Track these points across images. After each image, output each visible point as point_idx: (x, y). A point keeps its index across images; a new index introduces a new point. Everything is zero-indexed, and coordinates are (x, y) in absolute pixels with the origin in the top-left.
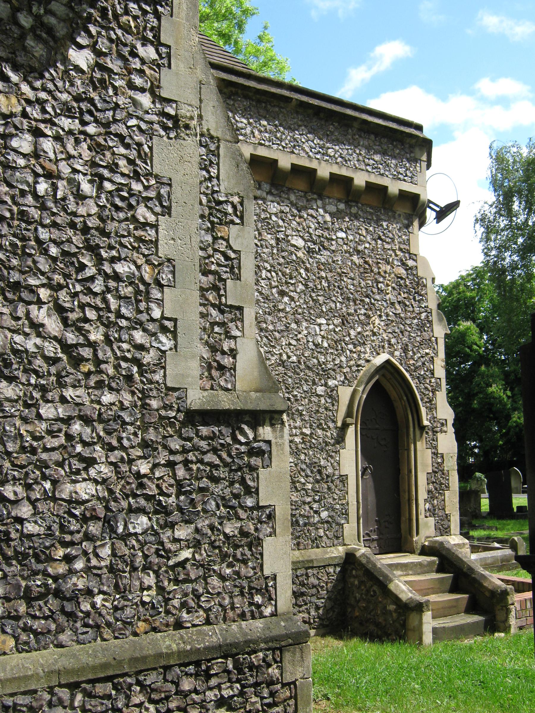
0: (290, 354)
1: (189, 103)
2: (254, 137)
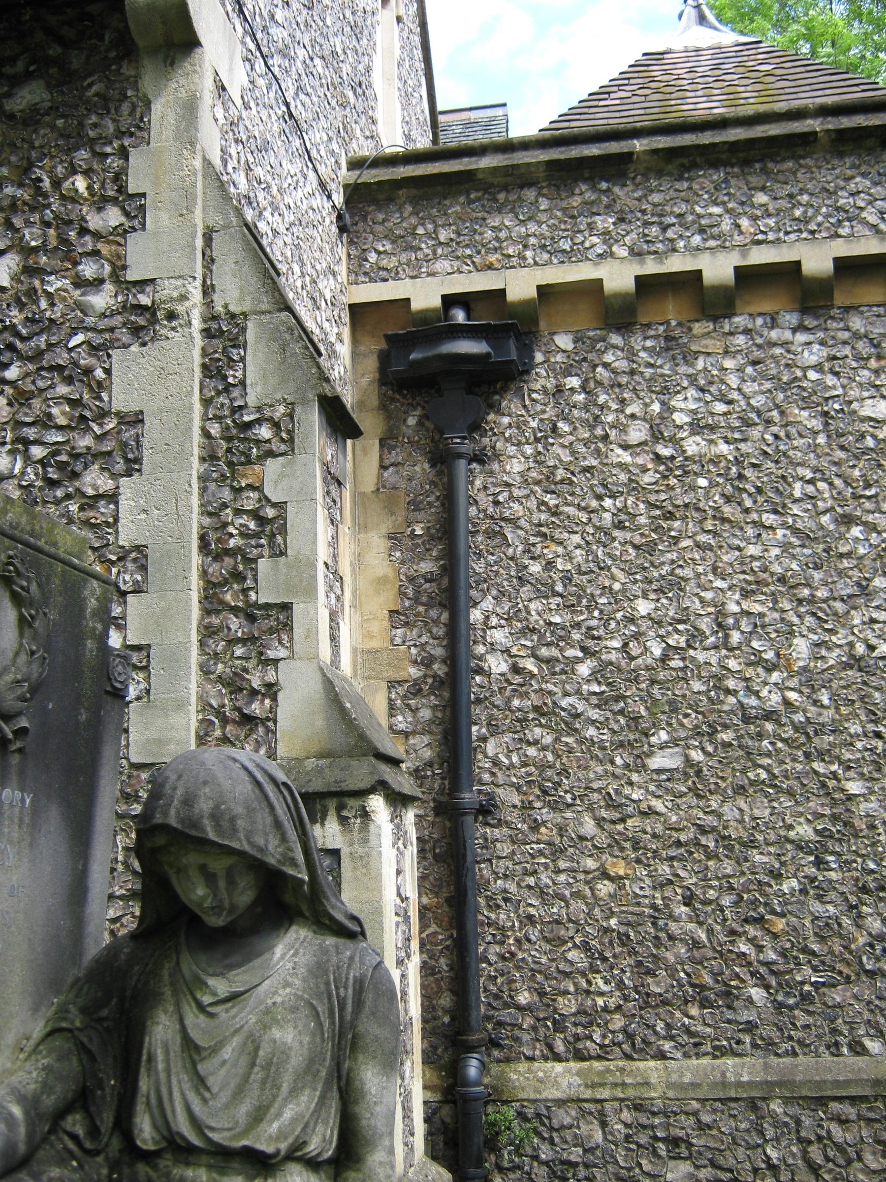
0: (874, 641)
1: (177, 274)
2: (741, 233)
